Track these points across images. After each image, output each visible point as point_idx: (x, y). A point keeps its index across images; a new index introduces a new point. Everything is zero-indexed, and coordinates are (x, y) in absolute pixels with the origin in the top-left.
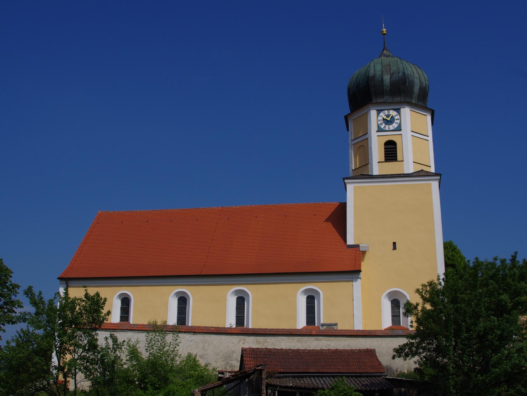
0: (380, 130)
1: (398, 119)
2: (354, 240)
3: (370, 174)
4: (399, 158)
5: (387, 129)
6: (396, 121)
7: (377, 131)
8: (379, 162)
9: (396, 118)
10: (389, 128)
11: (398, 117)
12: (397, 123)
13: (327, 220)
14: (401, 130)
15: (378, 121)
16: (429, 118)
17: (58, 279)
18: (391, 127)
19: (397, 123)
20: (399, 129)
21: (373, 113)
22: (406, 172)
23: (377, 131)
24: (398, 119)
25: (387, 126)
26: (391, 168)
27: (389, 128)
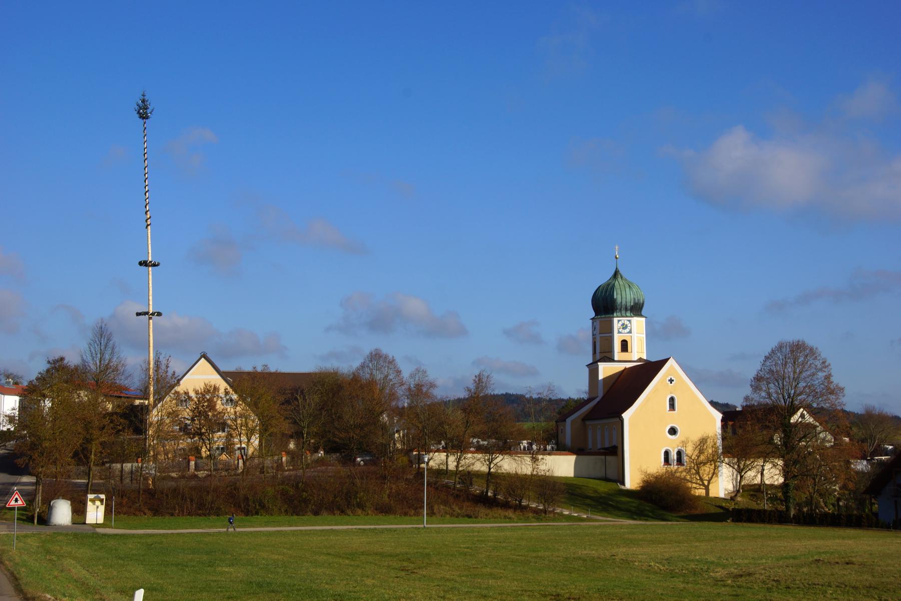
0: (619, 332)
4: (629, 350)
16: (591, 361)
20: (630, 332)
21: (616, 320)
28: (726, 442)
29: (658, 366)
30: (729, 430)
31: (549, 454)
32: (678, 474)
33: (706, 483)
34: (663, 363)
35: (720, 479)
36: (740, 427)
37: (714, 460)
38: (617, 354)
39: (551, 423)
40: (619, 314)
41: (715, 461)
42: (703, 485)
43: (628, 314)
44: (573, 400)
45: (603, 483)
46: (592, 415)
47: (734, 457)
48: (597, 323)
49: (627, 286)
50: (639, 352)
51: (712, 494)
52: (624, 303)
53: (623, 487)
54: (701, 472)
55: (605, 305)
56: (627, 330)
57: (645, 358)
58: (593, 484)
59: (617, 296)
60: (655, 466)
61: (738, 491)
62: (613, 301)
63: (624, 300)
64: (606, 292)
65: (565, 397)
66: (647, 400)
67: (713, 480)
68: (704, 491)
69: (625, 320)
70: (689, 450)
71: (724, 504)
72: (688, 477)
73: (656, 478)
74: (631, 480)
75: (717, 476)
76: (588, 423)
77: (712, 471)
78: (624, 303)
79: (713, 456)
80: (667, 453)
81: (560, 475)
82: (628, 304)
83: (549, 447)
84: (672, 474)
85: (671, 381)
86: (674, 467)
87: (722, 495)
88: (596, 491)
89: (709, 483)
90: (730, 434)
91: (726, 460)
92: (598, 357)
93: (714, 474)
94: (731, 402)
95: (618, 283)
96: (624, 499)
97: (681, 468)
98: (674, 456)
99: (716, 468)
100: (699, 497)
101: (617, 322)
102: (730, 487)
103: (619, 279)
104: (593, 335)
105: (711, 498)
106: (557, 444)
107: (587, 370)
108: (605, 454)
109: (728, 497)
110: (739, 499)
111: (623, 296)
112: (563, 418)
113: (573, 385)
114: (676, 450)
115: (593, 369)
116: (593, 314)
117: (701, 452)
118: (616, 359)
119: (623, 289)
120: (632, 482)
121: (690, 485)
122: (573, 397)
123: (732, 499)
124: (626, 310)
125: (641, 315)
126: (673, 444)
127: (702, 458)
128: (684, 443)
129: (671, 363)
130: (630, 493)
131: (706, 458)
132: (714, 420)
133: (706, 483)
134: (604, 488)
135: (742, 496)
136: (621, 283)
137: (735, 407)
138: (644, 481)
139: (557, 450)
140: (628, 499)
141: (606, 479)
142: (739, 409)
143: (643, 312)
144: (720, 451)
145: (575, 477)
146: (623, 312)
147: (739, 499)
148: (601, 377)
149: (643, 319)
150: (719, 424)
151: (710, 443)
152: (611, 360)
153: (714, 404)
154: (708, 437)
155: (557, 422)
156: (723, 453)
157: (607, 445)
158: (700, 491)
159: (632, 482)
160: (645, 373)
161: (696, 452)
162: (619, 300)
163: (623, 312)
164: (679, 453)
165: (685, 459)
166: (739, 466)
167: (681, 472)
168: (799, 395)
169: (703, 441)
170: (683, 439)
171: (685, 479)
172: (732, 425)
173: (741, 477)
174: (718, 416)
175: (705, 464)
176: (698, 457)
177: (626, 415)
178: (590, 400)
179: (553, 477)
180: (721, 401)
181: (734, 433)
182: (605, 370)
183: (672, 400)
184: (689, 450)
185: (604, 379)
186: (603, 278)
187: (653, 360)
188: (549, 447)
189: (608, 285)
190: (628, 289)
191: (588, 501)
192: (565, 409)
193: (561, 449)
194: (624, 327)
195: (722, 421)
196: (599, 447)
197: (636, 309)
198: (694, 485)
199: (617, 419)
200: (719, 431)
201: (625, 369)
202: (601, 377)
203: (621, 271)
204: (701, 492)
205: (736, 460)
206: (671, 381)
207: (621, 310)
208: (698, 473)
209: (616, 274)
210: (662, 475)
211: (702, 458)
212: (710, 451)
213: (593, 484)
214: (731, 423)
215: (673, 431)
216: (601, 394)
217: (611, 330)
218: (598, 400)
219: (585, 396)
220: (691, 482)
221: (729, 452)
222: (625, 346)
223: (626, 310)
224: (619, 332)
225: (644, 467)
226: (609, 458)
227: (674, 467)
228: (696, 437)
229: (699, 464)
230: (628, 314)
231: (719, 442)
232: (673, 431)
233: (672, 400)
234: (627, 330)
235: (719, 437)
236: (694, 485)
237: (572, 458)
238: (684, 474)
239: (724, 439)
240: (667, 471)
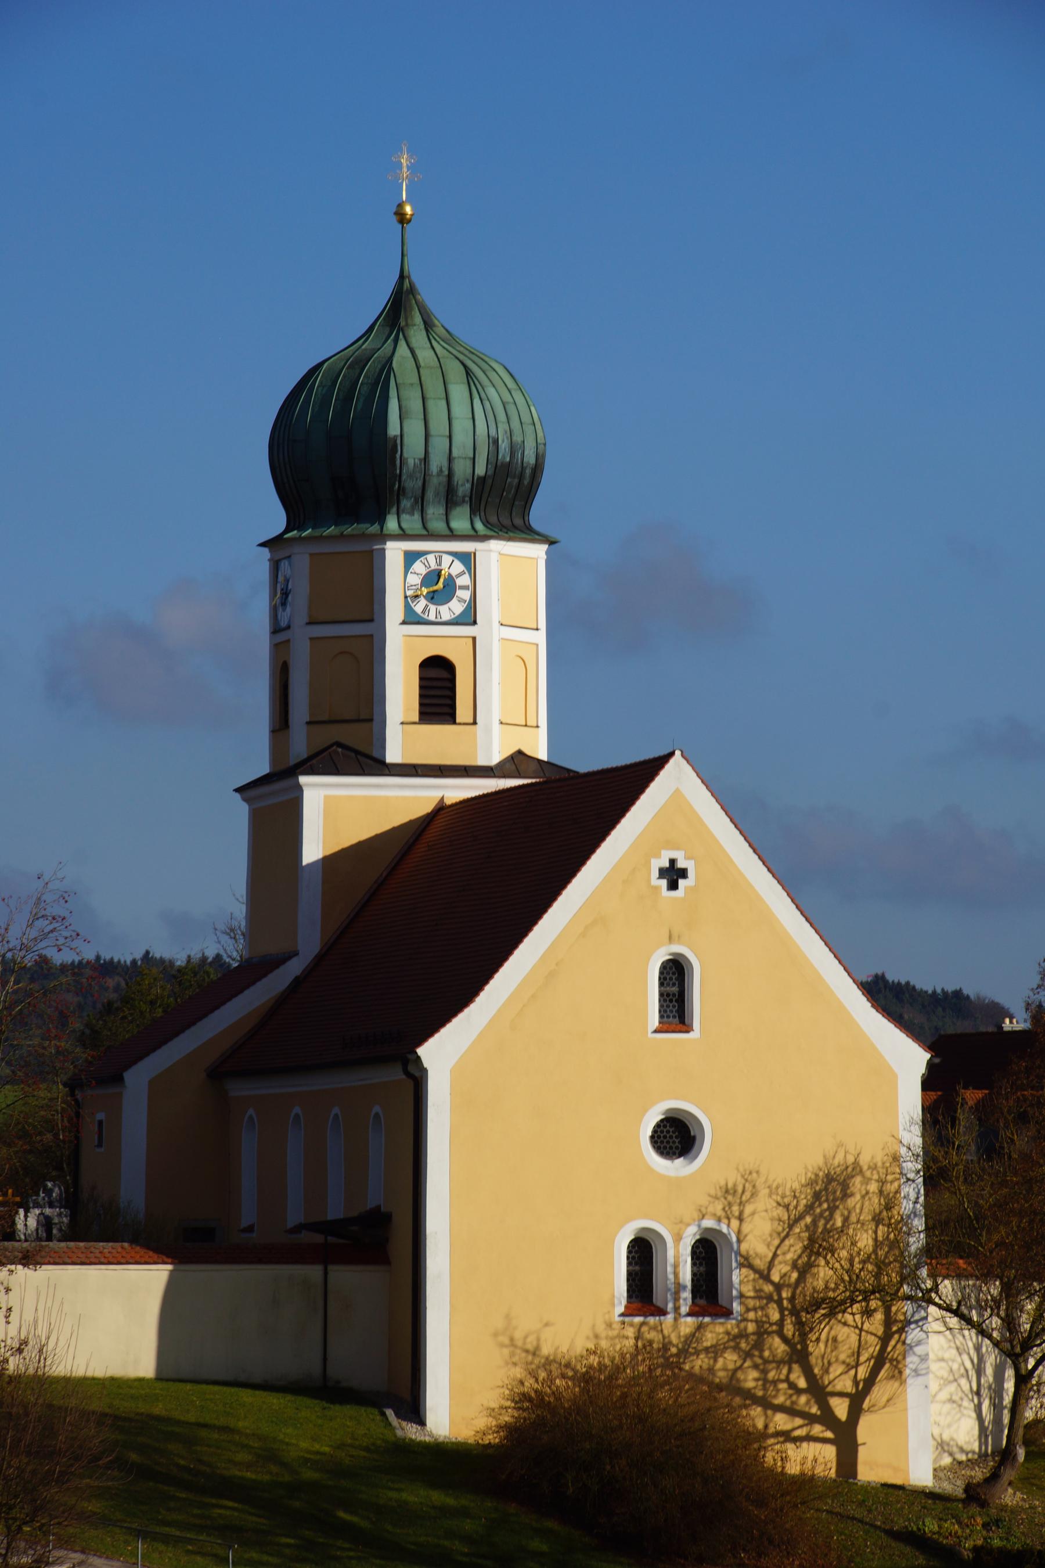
0: (411, 618)
1: (466, 588)
2: (419, 1058)
3: (376, 754)
4: (463, 712)
5: (432, 617)
6: (459, 593)
7: (404, 623)
8: (402, 723)
9: (459, 582)
10: (438, 613)
11: (465, 580)
12: (461, 600)
14: (475, 623)
15: (439, 555)
16: (264, 769)
17: (237, 790)
19: (461, 600)
20: (469, 617)
21: (394, 552)
22: (482, 761)
23: (404, 623)
24: (466, 588)
25: (433, 608)
26: (438, 743)
27: (438, 613)
28: (948, 1199)
29: (615, 791)
30: (965, 1131)
31: (28, 1259)
32: (698, 1363)
33: (841, 1408)
34: (631, 781)
35: (913, 1388)
36: (1023, 1118)
37: (885, 1290)
38: (402, 734)
39: (43, 1093)
40: (412, 522)
41: (889, 1296)
42: (827, 1418)
43: (460, 522)
44: (165, 966)
45: (309, 1410)
46: (270, 1049)
47: (986, 1276)
48: (299, 568)
49: (454, 371)
50: (510, 720)
51: (873, 1468)
52: (438, 461)
53: (411, 1431)
54: (817, 1350)
55: (341, 470)
56: (455, 607)
57: (543, 756)
58: (257, 1413)
59: (404, 425)
60: (584, 1317)
61: (1005, 1456)
62: (384, 450)
63: (439, 445)
64: (347, 399)
65: (127, 953)
66: (549, 972)
67: (880, 1392)
68: (829, 1452)
69: (440, 555)
70: (758, 1234)
71: (931, 1526)
72: (750, 1379)
73: (586, 1379)
74: (456, 1391)
75: (897, 1374)
76: (239, 1089)
77: (873, 1346)
78: (438, 461)
79: (881, 1267)
80: (642, 1251)
81: (80, 1370)
82: (462, 470)
83: (27, 1222)
84: (668, 1360)
85: (673, 875)
86: (678, 1324)
87: (920, 1473)
88: (269, 1454)
89: (857, 1401)
90: (970, 1155)
91: (947, 1288)
92: (299, 746)
93: (880, 1361)
94: (976, 986)
95: (413, 355)
96: (416, 1495)
97: (716, 1331)
98: (677, 1263)
99: (894, 1329)
100: (805, 1483)
101: (401, 567)
102: (965, 1433)
103: (417, 335)
104: (276, 629)
105: (869, 1490)
106: (71, 1202)
107: (240, 812)
108: (325, 1256)
109: (954, 1488)
110: (1010, 1497)
111: (437, 423)
112: (104, 1069)
113: (165, 890)
114: (690, 1235)
115: (274, 813)
116: (274, 519)
117: (818, 1245)
118: (393, 755)
119: (433, 386)
120: (458, 1400)
121: (757, 1417)
122: (161, 951)
123: (974, 1495)
124: (450, 500)
125: (524, 532)
126: (675, 1200)
127: (823, 1274)
128: (734, 1198)
129: (677, 779)
130: (449, 1461)
131: (843, 1279)
132: (887, 1077)
133: (841, 1408)
134: (311, 1433)
135: (1026, 1482)
136: (425, 355)
137: (999, 1012)
138: (522, 1399)
139: (73, 1234)
140: (438, 1497)
141: (328, 1390)
142: (1016, 1023)
143: (538, 514)
144: (916, 1242)
145: (161, 1377)
146: (435, 512)
147: (1010, 1497)
148: (312, 851)
149: (538, 551)
150: (910, 1100)
151: (862, 1201)
152: (369, 761)
153: (887, 995)
154: (856, 1168)
155: (73, 1085)
156: (928, 1251)
157: (335, 1210)
158: (810, 1450)
159: (458, 1400)
160: (538, 832)
161: (794, 1248)
162: (413, 448)
163: (435, 512)
164: (706, 1252)
165: (737, 1280)
166: (1010, 1323)
167: (715, 1351)
168: (852, 1265)
169: (831, 1188)
170: (733, 1178)
171: (733, 1386)
172: (981, 1110)
173: (1022, 1380)
174: (908, 1060)
175: (835, 1308)
176: (804, 1270)
177: (441, 1054)
178: (253, 970)
179: (41, 1382)
180: (928, 980)
181: (990, 1147)
182: (337, 814)
183: (675, 973)
184: (758, 1234)
185: (329, 862)
186: (333, 325)
187: (584, 764)
188: (27, 1222)
189: (360, 363)
190: (459, 391)
191: (227, 1510)
192: (129, 1009)
193: (93, 1229)
194: (438, 587)
195: (927, 1084)
196: (293, 1219)
197: (503, 498)
198: (781, 1421)
199: (394, 1074)
200: (913, 1137)
201: (441, 809)
202: (312, 851)
203: (428, 292)
204: (815, 1457)
205: (995, 1289)
206: (673, 875)
207: (420, 503)
208: (799, 1356)
209: (400, 307)
210: (618, 1369)
211: (823, 1274)
212: (865, 1241)
213: (257, 1413)
214: (972, 1096)
215: (676, 1136)
216: (309, 942)
217: (371, 611)
218: (295, 968)
219: (233, 951)
220: (766, 1404)
221: (960, 1250)
222: (439, 690)
223: (450, 500)
224: (411, 618)
225: (525, 1325)
226: (346, 1278)
227: (678, 1324)
228: (792, 1168)
229: (808, 1310)
230: (460, 522)
231: (911, 1196)
232: (676, 1136)
233: (675, 973)
234: (455, 607)
235: (913, 1167)
236: (781, 1421)
237: (151, 1280)
238: (730, 1359)
239: (935, 1177)
240: (642, 1348)
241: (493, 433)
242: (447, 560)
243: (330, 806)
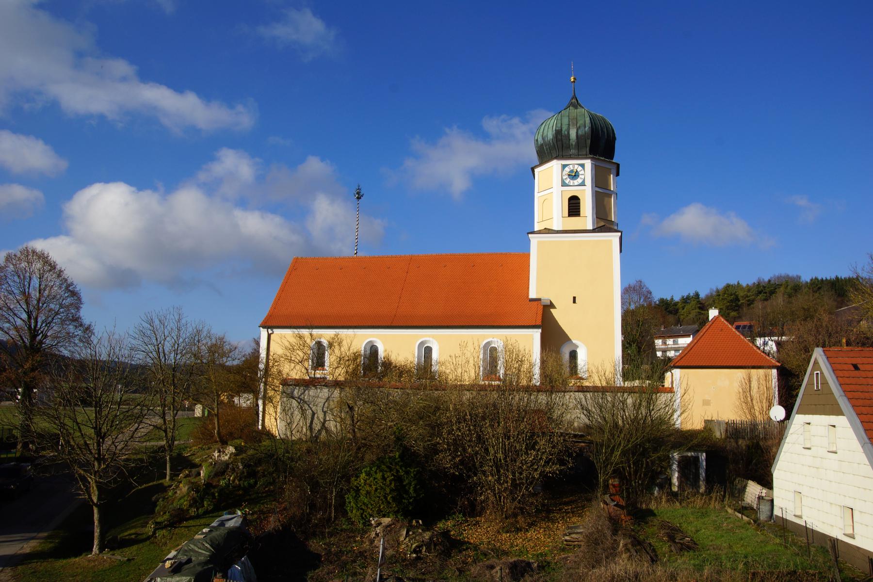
13: (593, 119)
18: (576, 182)
26: (574, 223)
56: (579, 181)
183: (574, 298)
233: (574, 298)
241: (545, 134)
242: (576, 166)
243: (539, 242)
